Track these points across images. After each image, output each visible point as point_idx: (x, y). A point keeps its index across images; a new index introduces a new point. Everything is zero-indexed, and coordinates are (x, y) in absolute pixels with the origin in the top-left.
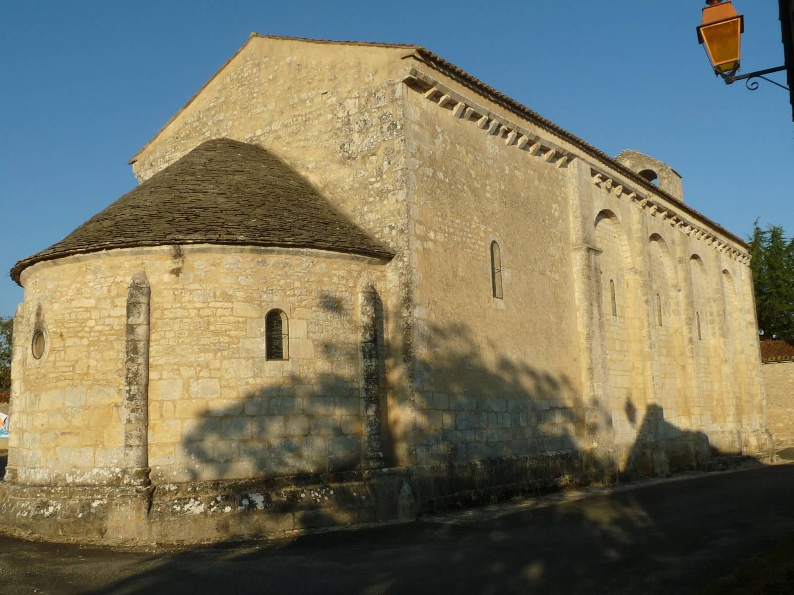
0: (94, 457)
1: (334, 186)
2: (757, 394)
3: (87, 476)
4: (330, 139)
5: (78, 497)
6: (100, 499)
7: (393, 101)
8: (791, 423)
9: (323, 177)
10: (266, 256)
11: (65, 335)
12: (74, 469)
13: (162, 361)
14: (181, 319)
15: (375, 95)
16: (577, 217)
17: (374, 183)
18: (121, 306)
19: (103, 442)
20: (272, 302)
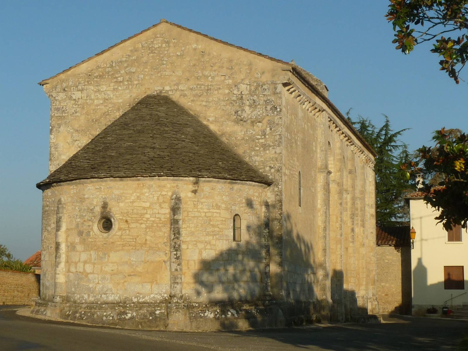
0: (151, 288)
1: (230, 135)
2: (372, 271)
3: (147, 298)
4: (227, 105)
5: (145, 309)
6: (159, 310)
7: (275, 93)
8: (383, 295)
9: (221, 128)
10: (234, 185)
11: (129, 221)
12: (138, 295)
13: (188, 239)
14: (198, 217)
15: (262, 87)
16: (322, 151)
17: (260, 139)
18: (165, 208)
19: (156, 281)
20: (235, 210)
